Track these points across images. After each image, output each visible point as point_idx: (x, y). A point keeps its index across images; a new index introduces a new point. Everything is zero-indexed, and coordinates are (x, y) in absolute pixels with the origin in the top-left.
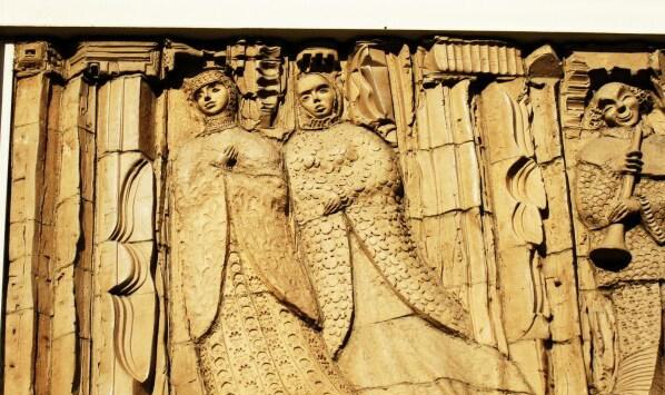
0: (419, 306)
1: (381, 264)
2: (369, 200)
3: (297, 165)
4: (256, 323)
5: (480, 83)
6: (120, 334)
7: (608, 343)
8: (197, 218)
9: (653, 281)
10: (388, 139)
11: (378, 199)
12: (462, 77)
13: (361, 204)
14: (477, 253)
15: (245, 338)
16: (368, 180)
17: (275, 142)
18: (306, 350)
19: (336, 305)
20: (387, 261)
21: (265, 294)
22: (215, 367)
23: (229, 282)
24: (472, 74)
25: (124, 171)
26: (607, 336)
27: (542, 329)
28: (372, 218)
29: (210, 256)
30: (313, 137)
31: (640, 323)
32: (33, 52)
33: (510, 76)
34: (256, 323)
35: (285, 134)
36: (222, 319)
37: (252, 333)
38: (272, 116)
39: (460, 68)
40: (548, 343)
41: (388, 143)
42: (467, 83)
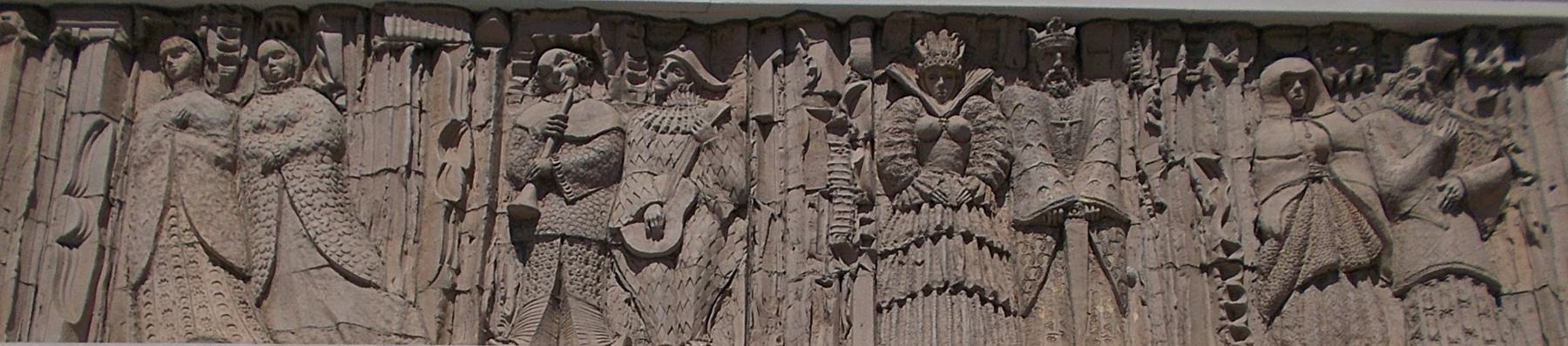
0: (334, 258)
2: (305, 158)
3: (248, 126)
4: (183, 272)
6: (62, 281)
9: (555, 237)
11: (313, 158)
12: (408, 43)
16: (305, 140)
19: (262, 255)
20: (311, 216)
21: (196, 245)
22: (144, 311)
24: (418, 40)
25: (84, 133)
29: (151, 209)
30: (267, 100)
31: (541, 274)
32: (9, 18)
33: (455, 42)
34: (183, 272)
35: (243, 98)
36: (154, 267)
37: (180, 280)
38: (232, 83)
40: (452, 293)
41: (337, 106)
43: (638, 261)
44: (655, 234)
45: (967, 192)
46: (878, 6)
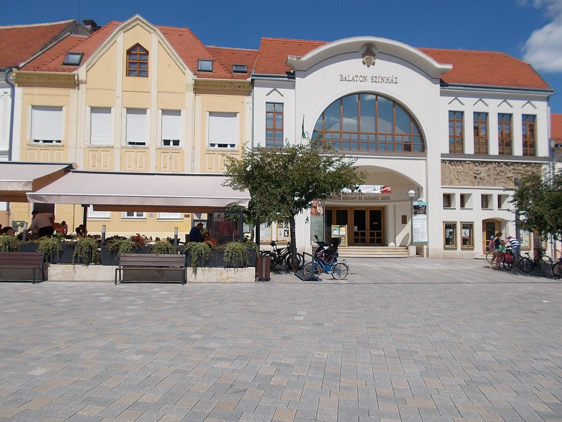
5: (469, 163)
43: (482, 180)
44: (484, 178)
45: (118, 271)
46: (47, 110)
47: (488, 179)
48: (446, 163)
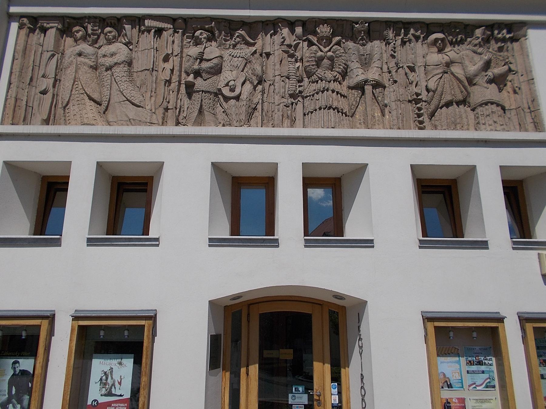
0: (129, 98)
1: (119, 85)
3: (101, 55)
5: (159, 32)
7: (185, 110)
8: (68, 71)
9: (200, 91)
10: (130, 47)
11: (122, 66)
13: (116, 67)
14: (150, 82)
15: (76, 106)
16: (119, 60)
17: (96, 49)
18: (94, 110)
20: (121, 84)
23: (74, 90)
24: (156, 27)
25: (48, 58)
26: (186, 107)
27: (165, 104)
28: (119, 71)
34: (80, 102)
35: (99, 46)
39: (152, 25)
40: (167, 109)
41: (129, 49)
42: (153, 30)
43: (227, 99)
44: (232, 90)
47: (258, 97)
48: (44, 30)
